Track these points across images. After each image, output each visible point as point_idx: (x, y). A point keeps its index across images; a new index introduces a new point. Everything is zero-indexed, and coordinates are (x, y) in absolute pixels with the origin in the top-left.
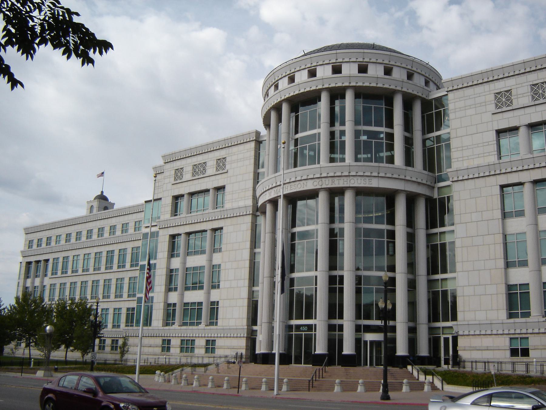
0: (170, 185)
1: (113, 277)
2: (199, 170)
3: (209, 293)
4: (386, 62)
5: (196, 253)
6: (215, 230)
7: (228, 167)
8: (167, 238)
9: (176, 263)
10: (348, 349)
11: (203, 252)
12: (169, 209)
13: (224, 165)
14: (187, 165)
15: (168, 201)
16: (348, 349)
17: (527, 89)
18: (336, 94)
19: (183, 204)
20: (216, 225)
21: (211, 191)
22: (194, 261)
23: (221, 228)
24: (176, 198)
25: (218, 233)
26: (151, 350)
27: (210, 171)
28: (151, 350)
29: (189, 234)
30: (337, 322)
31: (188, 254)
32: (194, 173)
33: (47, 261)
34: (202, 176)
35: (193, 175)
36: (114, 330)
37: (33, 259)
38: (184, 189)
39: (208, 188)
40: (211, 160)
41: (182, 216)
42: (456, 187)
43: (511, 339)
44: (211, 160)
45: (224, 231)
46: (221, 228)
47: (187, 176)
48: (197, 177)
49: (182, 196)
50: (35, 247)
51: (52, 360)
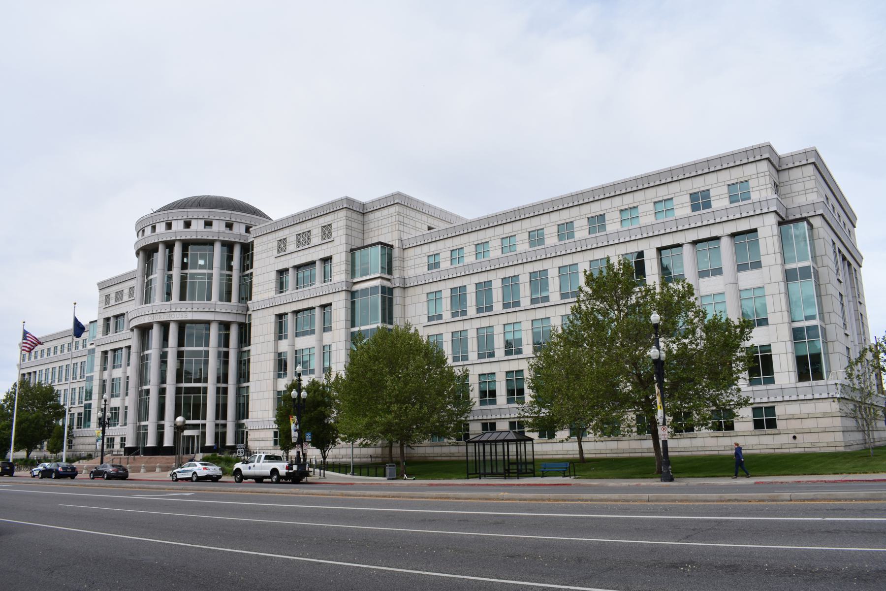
0: (273, 259)
1: (471, 329)
2: (304, 239)
3: (124, 400)
4: (206, 217)
5: (305, 333)
6: (324, 307)
7: (334, 235)
8: (273, 318)
9: (106, 375)
10: (168, 442)
11: (312, 332)
12: (273, 285)
13: (330, 232)
14: (290, 235)
15: (101, 323)
16: (168, 442)
17: (294, 238)
18: (170, 245)
19: (290, 277)
20: (324, 301)
21: (317, 263)
22: (303, 343)
23: (330, 304)
24: (282, 272)
25: (327, 309)
26: (262, 444)
27: (316, 240)
28: (262, 444)
29: (296, 312)
30: (143, 423)
31: (114, 367)
32: (299, 243)
33: (35, 372)
34: (307, 246)
35: (298, 246)
36: (483, 407)
37: (25, 371)
38: (289, 262)
39: (314, 259)
40: (315, 227)
41: (287, 293)
42: (254, 316)
43: (753, 409)
44: (315, 227)
45: (333, 307)
46: (330, 304)
47: (291, 247)
48: (301, 248)
49: (287, 270)
50: (45, 356)
51: (677, 457)
